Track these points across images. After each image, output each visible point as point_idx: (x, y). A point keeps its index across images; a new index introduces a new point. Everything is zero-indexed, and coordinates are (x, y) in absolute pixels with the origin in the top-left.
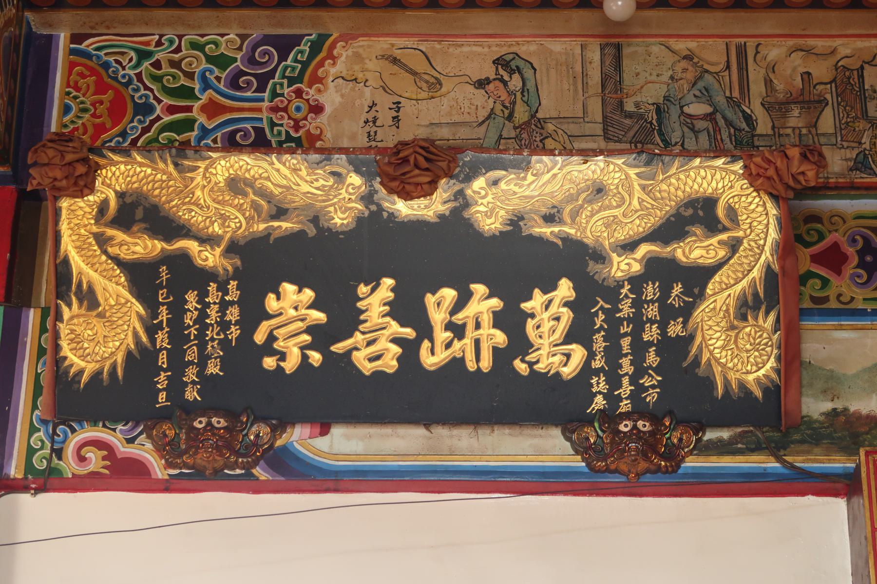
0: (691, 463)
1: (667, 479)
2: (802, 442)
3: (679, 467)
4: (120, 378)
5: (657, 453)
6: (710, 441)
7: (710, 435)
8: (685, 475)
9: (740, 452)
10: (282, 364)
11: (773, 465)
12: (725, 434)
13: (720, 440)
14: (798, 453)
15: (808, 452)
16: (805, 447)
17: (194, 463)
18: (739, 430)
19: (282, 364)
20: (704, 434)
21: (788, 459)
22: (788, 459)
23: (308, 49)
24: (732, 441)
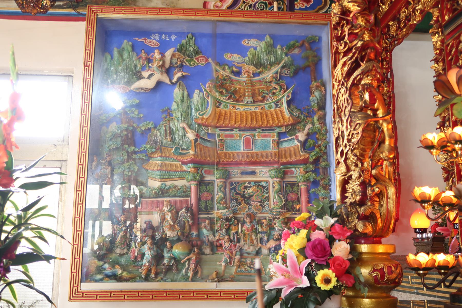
0: (51, 11)
1: (44, 15)
2: (82, 6)
3: (47, 12)
4: (136, 39)
5: (39, 7)
6: (57, 5)
7: (57, 3)
8: (49, 14)
9: (65, 8)
10: (337, 241)
11: (73, 12)
12: (61, 3)
13: (60, 5)
14: (81, 9)
15: (84, 9)
16: (83, 7)
17: (304, 182)
18: (65, 2)
19: (337, 241)
20: (55, 3)
21: (78, 10)
22: (78, 10)
23: (193, 114)
24: (63, 5)
